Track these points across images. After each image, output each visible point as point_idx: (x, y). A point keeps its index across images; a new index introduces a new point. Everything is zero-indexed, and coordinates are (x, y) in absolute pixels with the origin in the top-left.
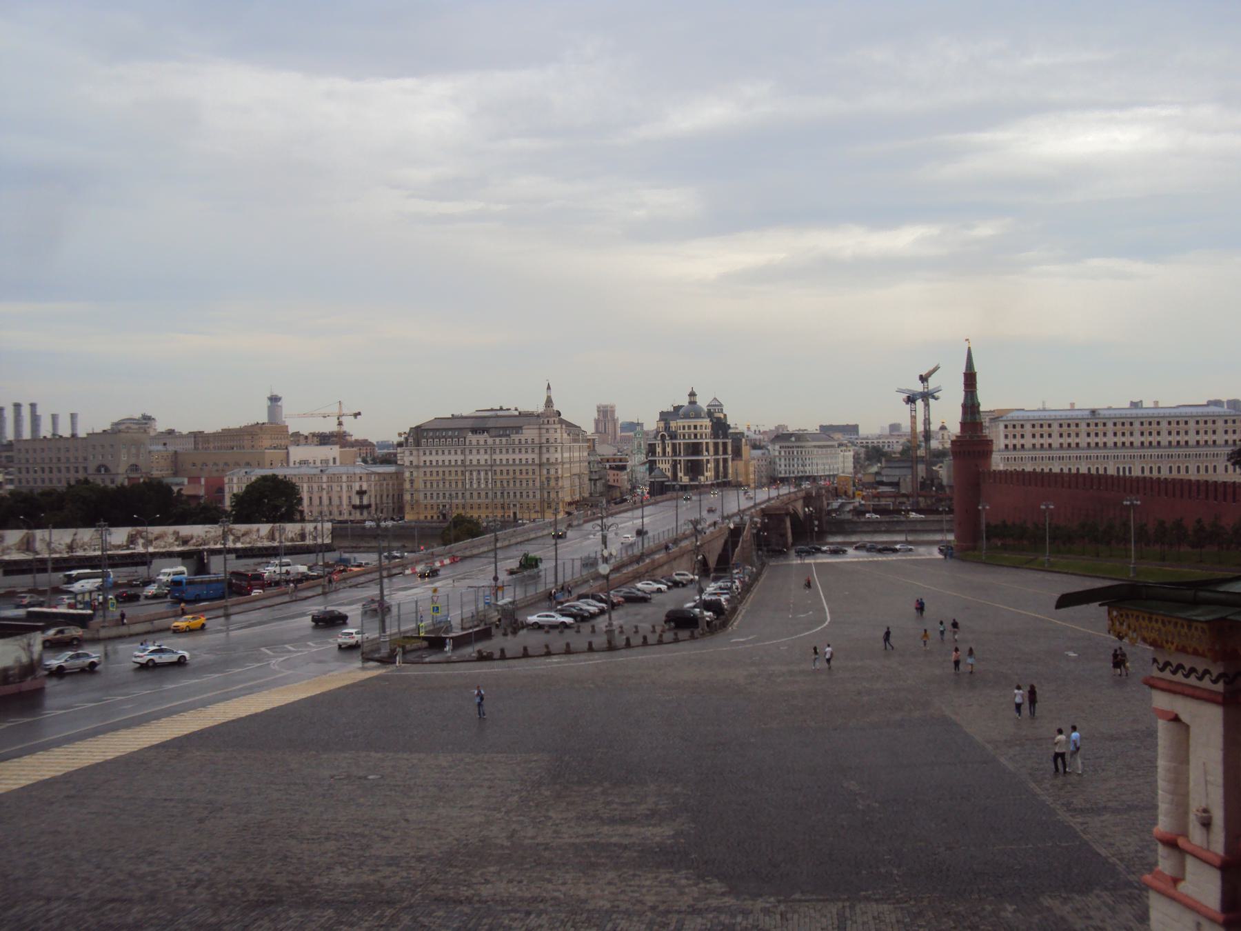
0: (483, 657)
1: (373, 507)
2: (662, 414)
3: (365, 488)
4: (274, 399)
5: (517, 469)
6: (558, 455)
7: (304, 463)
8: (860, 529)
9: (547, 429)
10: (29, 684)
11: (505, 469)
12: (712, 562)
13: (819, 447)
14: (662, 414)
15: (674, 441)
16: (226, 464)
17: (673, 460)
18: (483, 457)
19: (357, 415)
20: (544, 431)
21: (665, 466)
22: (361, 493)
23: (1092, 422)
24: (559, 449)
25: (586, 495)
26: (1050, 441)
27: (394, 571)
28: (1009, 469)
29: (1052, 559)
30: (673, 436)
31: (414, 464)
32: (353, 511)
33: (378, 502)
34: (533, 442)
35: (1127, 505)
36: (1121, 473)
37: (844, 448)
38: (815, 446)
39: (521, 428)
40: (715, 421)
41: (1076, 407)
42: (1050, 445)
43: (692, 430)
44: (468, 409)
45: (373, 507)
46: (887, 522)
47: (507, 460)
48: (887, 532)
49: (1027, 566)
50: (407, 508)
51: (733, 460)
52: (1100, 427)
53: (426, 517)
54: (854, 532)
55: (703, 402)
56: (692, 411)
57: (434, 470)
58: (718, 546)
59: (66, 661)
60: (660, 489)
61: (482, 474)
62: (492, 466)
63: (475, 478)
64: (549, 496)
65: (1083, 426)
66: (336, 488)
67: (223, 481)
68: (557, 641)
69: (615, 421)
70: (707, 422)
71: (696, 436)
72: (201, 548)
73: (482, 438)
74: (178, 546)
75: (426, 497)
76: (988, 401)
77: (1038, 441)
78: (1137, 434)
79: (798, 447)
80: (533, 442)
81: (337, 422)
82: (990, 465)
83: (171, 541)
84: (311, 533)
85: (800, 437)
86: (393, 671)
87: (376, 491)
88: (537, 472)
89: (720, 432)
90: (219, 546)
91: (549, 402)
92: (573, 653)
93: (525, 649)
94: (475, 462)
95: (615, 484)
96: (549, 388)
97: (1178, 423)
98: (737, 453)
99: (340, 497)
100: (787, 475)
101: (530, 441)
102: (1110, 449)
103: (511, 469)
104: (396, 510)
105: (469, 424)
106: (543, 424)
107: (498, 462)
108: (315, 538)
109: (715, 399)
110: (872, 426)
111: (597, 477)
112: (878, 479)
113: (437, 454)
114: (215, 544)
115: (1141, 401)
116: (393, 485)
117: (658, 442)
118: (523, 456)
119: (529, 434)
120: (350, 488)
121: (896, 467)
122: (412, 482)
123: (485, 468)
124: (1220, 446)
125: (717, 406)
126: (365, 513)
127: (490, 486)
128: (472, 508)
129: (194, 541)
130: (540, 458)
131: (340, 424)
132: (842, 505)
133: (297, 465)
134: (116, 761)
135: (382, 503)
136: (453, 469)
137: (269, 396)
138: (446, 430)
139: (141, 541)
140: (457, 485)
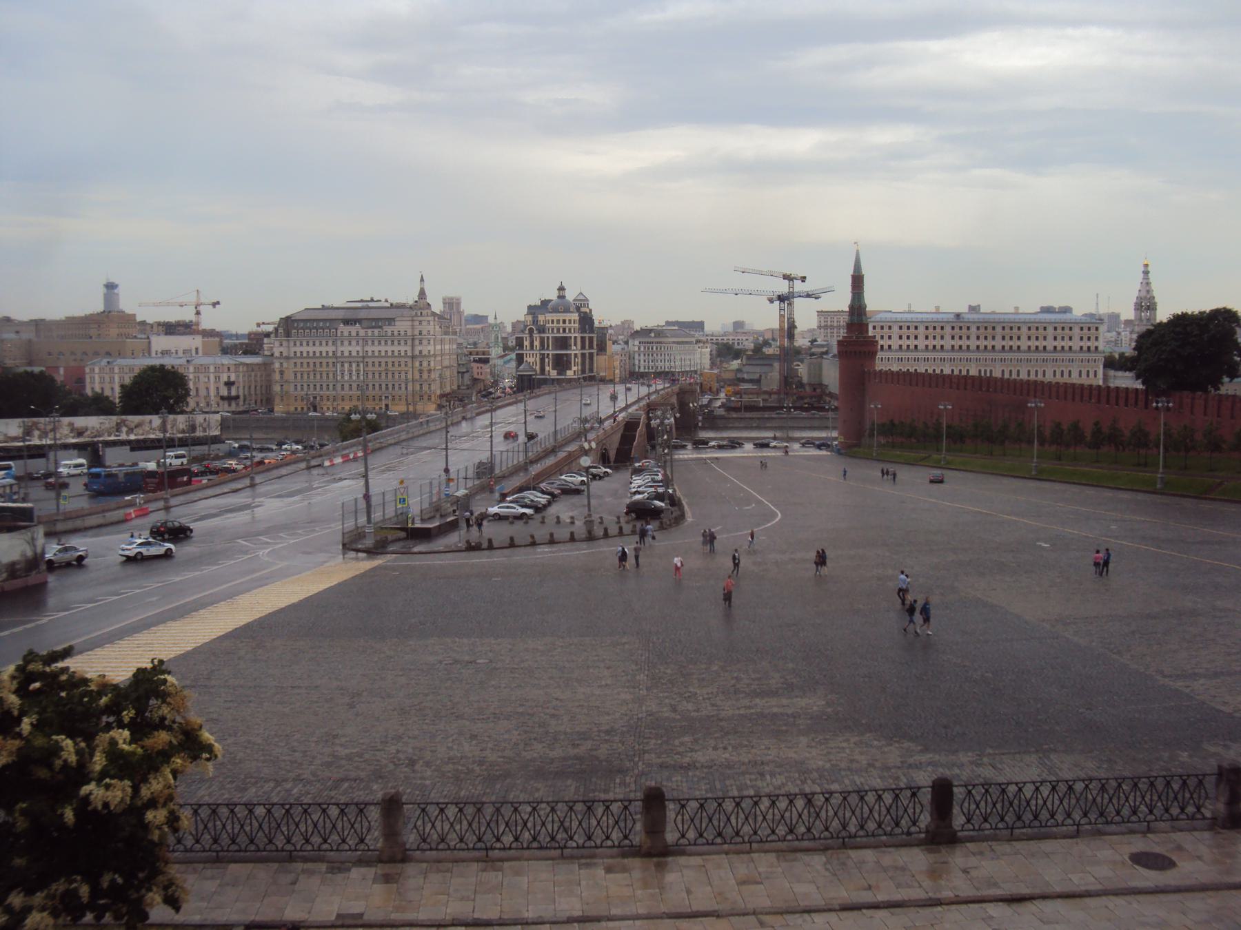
0: (472, 548)
1: (242, 398)
2: (530, 307)
3: (233, 379)
4: (111, 287)
5: (390, 360)
6: (431, 348)
7: (165, 353)
8: (731, 425)
9: (421, 321)
10: (33, 579)
11: (376, 361)
12: (612, 454)
13: (678, 343)
14: (530, 307)
15: (543, 335)
16: (85, 353)
17: (541, 354)
18: (355, 349)
19: (215, 304)
20: (417, 323)
21: (532, 359)
22: (229, 384)
23: (957, 325)
24: (432, 342)
25: (455, 387)
26: (916, 342)
27: (313, 463)
28: (884, 369)
29: (947, 457)
30: (542, 330)
31: (284, 355)
32: (221, 403)
33: (246, 393)
34: (406, 334)
35: (1031, 407)
36: (983, 374)
37: (701, 345)
38: (674, 342)
39: (393, 319)
40: (582, 315)
41: (1020, 311)
42: (1045, 347)
43: (561, 324)
44: (339, 302)
45: (242, 398)
46: (758, 418)
47: (386, 351)
48: (758, 428)
49: (920, 463)
50: (277, 400)
51: (597, 355)
52: (965, 330)
53: (296, 409)
54: (726, 428)
55: (570, 296)
56: (561, 305)
57: (305, 361)
58: (616, 439)
59: (55, 554)
60: (527, 385)
61: (354, 365)
62: (364, 357)
63: (346, 369)
64: (421, 388)
65: (948, 329)
66: (203, 379)
67: (84, 371)
68: (518, 529)
69: (460, 313)
70: (575, 316)
71: (564, 330)
72: (95, 439)
73: (353, 329)
74: (73, 437)
75: (296, 389)
76: (872, 302)
77: (905, 342)
78: (947, 337)
79: (658, 343)
80: (406, 334)
81: (195, 311)
82: (873, 365)
83: (66, 432)
84: (201, 425)
85: (658, 333)
86: (388, 561)
87: (244, 381)
88: (410, 365)
89: (587, 327)
90: (112, 438)
91: (422, 294)
92: (557, 543)
93: (512, 539)
94: (346, 354)
95: (480, 377)
96: (422, 280)
97: (882, 328)
98: (602, 348)
99: (207, 389)
100: (647, 370)
101: (402, 333)
102: (947, 352)
103: (383, 360)
104: (264, 401)
105: (340, 315)
106: (416, 315)
107: (370, 354)
108: (205, 430)
109: (581, 293)
110: (717, 322)
111: (464, 370)
112: (739, 376)
113: (308, 345)
114: (110, 436)
115: (979, 306)
116: (261, 376)
117: (526, 336)
118: (396, 348)
119: (402, 326)
120: (217, 379)
121: (757, 365)
122: (282, 373)
123: (357, 359)
124: (1075, 352)
125: (584, 300)
126: (233, 404)
127: (362, 378)
128: (343, 400)
129: (89, 433)
130: (413, 350)
131: (198, 313)
132: (710, 401)
133: (160, 355)
134: (196, 651)
135: (250, 394)
136: (324, 361)
137: (105, 283)
138: (318, 320)
139: (36, 433)
140: (328, 377)
